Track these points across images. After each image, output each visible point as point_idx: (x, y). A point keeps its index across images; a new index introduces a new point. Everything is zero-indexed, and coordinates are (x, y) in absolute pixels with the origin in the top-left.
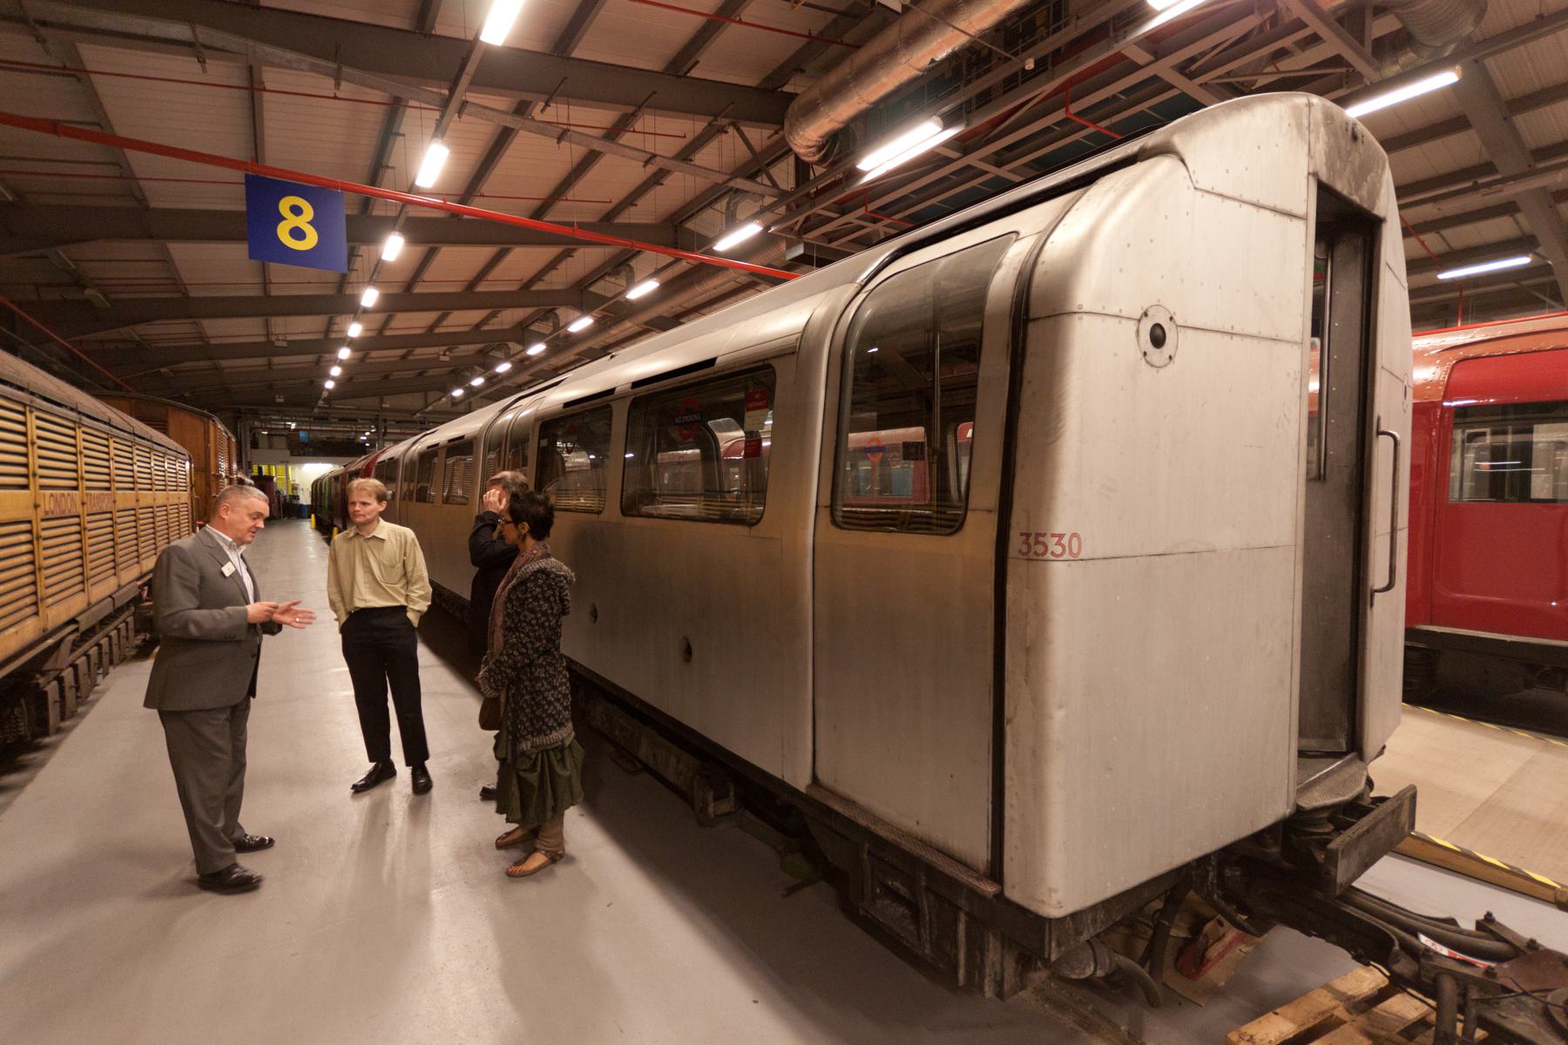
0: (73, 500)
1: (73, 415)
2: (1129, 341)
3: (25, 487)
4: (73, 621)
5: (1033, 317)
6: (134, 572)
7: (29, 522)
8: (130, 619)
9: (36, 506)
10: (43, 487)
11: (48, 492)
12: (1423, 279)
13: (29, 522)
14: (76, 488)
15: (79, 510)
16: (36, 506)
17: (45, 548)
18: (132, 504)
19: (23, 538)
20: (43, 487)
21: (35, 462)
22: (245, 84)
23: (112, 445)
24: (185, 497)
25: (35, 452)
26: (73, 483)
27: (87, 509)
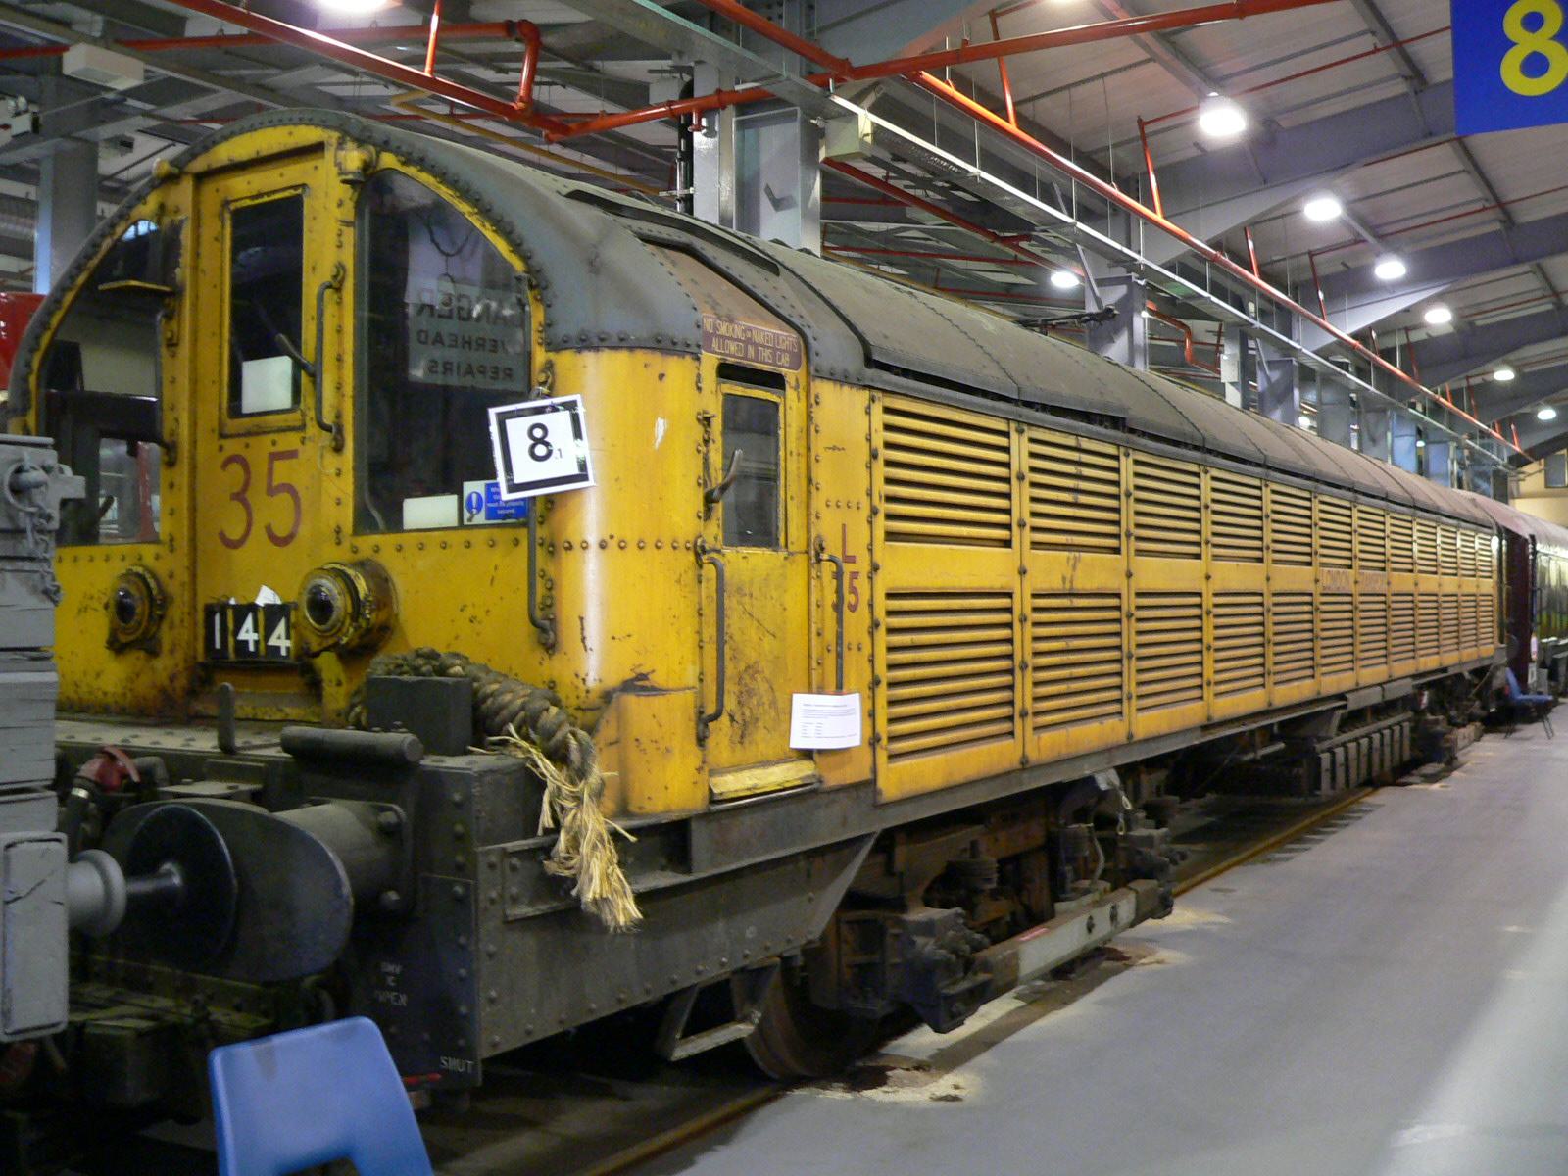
0: (1347, 578)
1: (1350, 494)
2: (333, 502)
3: (1309, 564)
4: (1341, 696)
5: (1526, 451)
6: (1379, 673)
7: (1311, 594)
8: (1407, 725)
9: (1317, 581)
10: (1324, 565)
11: (1327, 569)
12: (1465, 486)
13: (1311, 594)
14: (1350, 567)
15: (1352, 589)
16: (1317, 581)
17: (1324, 621)
18: (1473, 590)
19: (1307, 608)
20: (1324, 565)
21: (1317, 542)
22: (1406, 46)
23: (1388, 521)
24: (1488, 585)
25: (1317, 533)
26: (1347, 562)
27: (1361, 588)
